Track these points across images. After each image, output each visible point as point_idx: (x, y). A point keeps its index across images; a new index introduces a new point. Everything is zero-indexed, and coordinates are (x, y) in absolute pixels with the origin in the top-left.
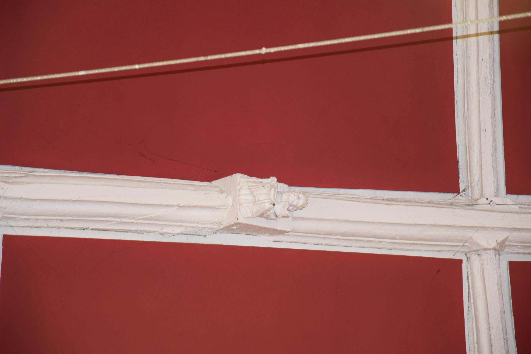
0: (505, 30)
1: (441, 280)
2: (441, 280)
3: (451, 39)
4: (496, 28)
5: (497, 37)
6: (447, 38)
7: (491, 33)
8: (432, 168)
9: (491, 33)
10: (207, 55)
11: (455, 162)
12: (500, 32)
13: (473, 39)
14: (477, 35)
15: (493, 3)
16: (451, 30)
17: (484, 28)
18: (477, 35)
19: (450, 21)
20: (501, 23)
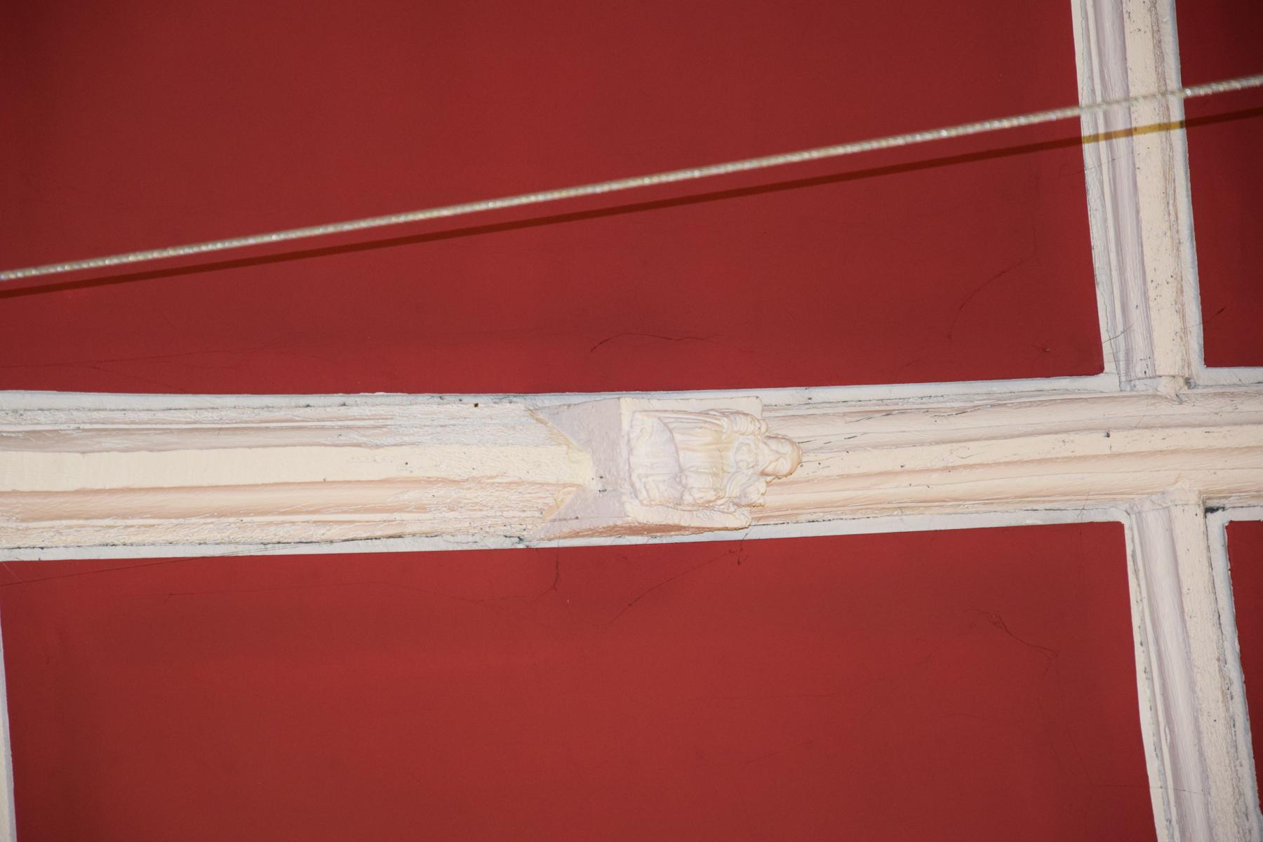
0: (1197, 119)
1: (1077, 569)
2: (1077, 569)
3: (1077, 141)
4: (1177, 115)
5: (1179, 138)
6: (1068, 140)
7: (1165, 127)
8: (1050, 331)
9: (1165, 127)
10: (164, 246)
11: (1147, 777)
12: (1188, 124)
13: (1121, 143)
14: (1109, 136)
15: (571, 537)
16: (1076, 121)
17: (1146, 114)
18: (1109, 136)
19: (1073, 100)
20: (1188, 103)
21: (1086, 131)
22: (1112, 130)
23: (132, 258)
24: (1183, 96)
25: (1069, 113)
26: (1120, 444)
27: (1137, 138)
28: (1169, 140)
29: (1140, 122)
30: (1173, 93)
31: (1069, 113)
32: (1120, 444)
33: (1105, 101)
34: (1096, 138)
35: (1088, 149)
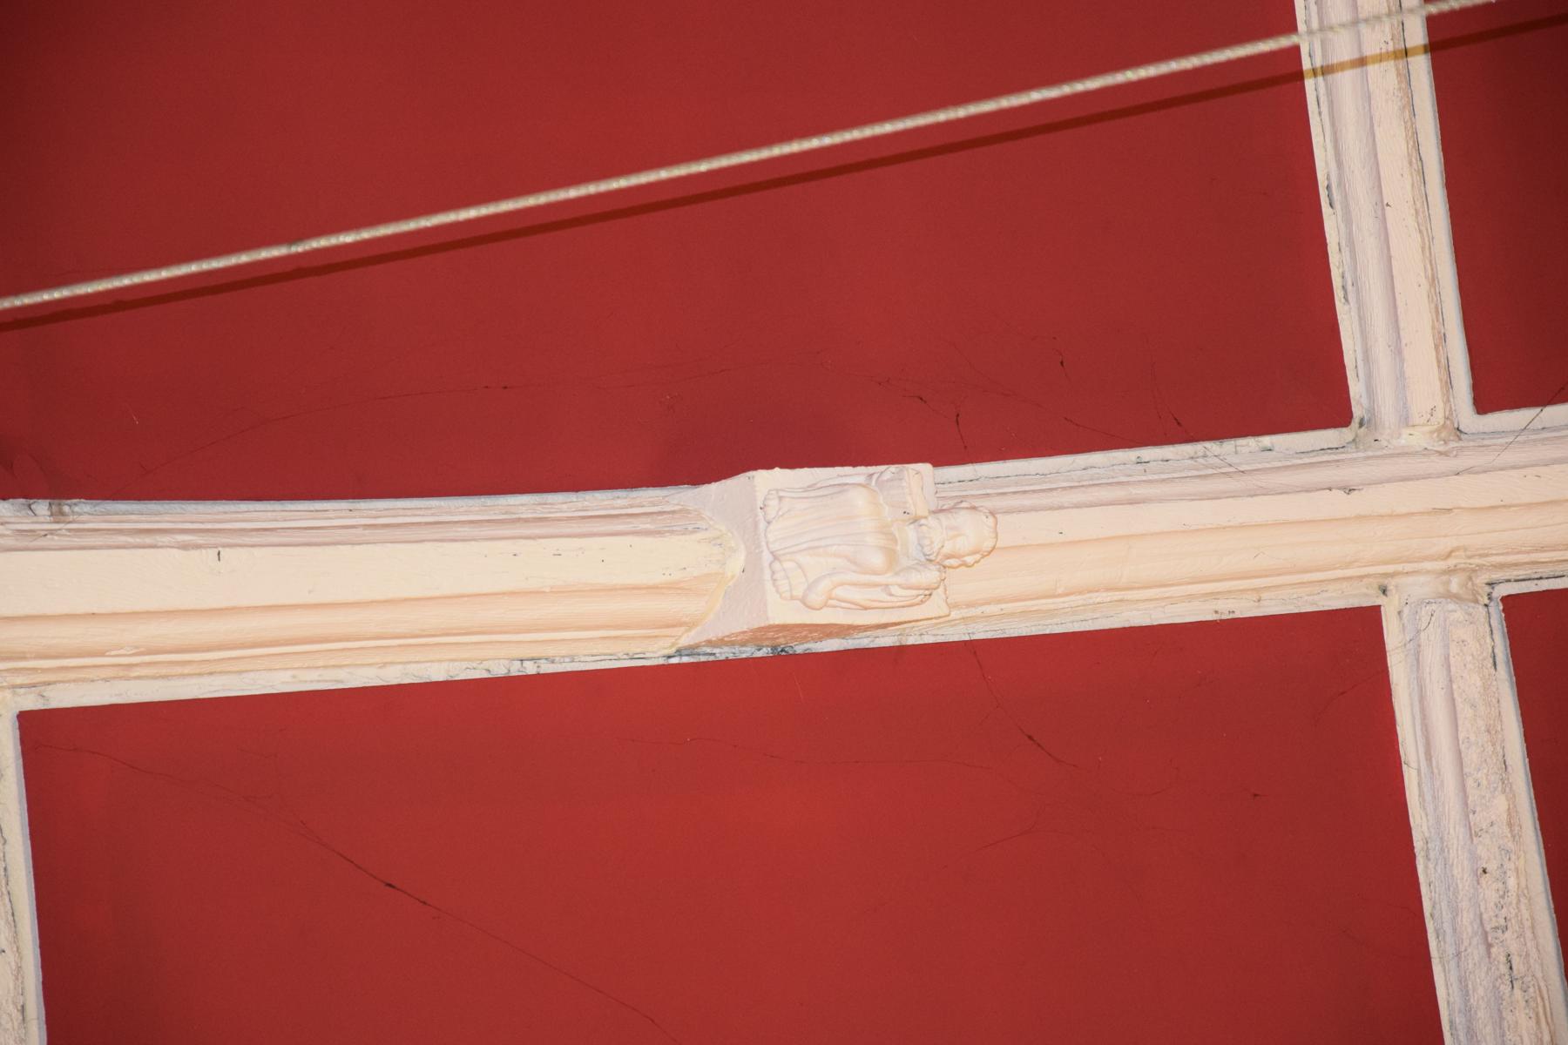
1: (1333, 661)
2: (1333, 661)
3: (1299, 76)
4: (1417, 35)
5: (1421, 67)
16: (1295, 51)
17: (1377, 40)
19: (1292, 28)
21: (1306, 65)
22: (1358, 70)
23: (265, 254)
24: (1424, 13)
25: (1283, 42)
26: (1390, 506)
27: (1372, 69)
28: (1324, 55)
29: (1370, 50)
30: (1411, 11)
31: (1283, 42)
32: (1390, 506)
33: (1321, 29)
34: (1314, 72)
35: (1309, 84)
